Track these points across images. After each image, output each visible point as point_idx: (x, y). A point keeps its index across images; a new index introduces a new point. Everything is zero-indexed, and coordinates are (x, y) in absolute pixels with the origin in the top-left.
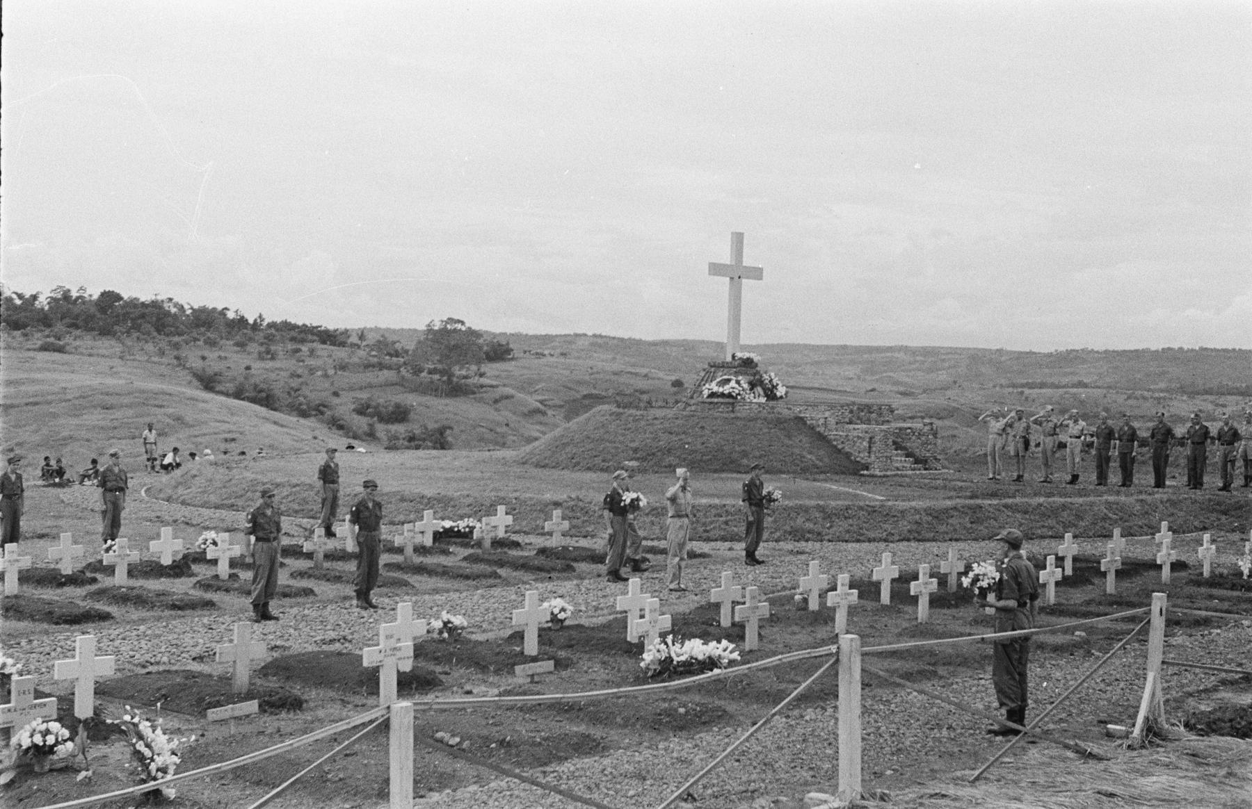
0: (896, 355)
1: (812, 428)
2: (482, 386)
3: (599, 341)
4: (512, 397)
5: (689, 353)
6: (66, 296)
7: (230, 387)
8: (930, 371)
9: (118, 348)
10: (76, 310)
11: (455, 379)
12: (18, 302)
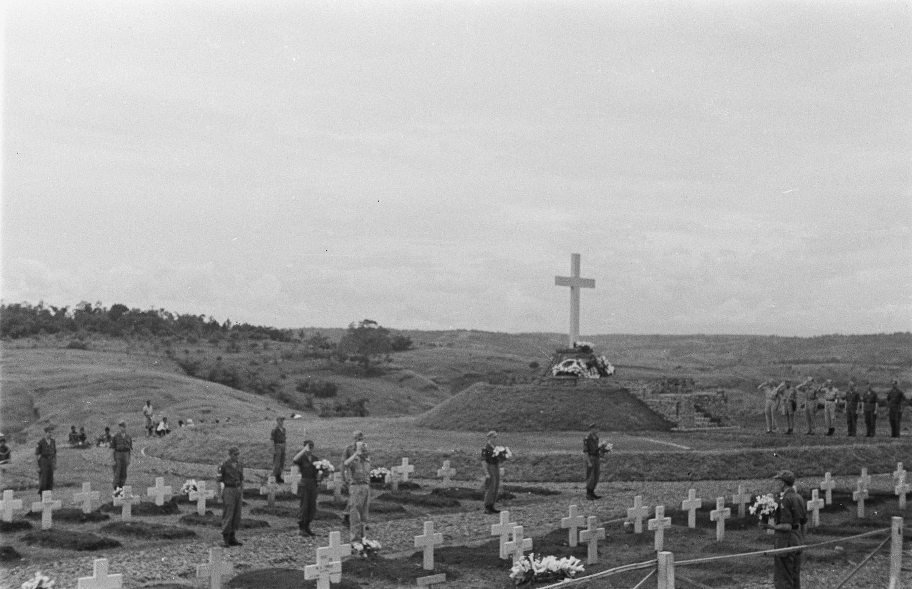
0: (696, 341)
1: (634, 397)
2: (390, 369)
6: (88, 307)
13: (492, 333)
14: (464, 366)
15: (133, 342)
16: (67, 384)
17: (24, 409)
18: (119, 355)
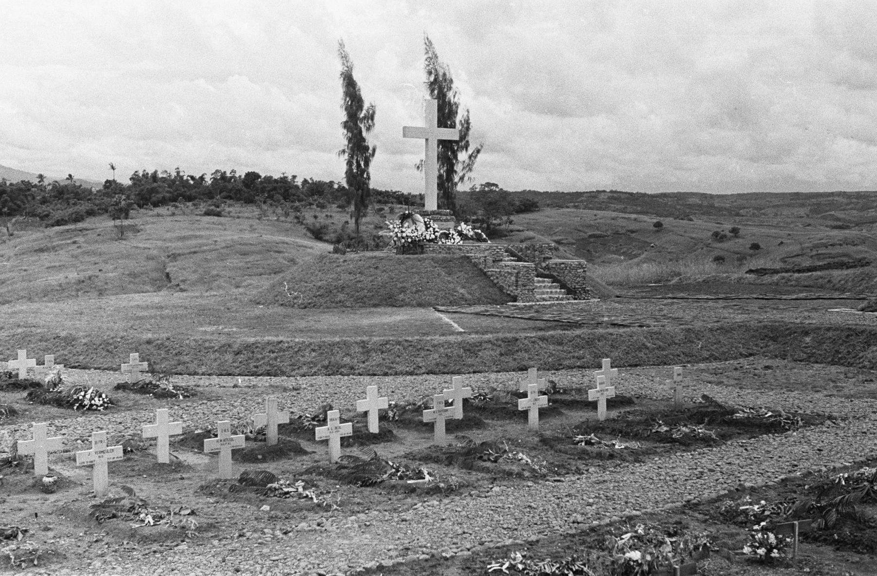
0: (836, 198)
1: (475, 265)
2: (512, 231)
3: (615, 195)
4: (534, 238)
5: (680, 202)
6: (223, 176)
7: (333, 236)
8: (862, 209)
9: (257, 212)
10: (230, 186)
11: (492, 226)
12: (192, 182)
13: (631, 194)
14: (590, 226)
15: (265, 207)
16: (197, 249)
17: (155, 275)
18: (251, 222)
